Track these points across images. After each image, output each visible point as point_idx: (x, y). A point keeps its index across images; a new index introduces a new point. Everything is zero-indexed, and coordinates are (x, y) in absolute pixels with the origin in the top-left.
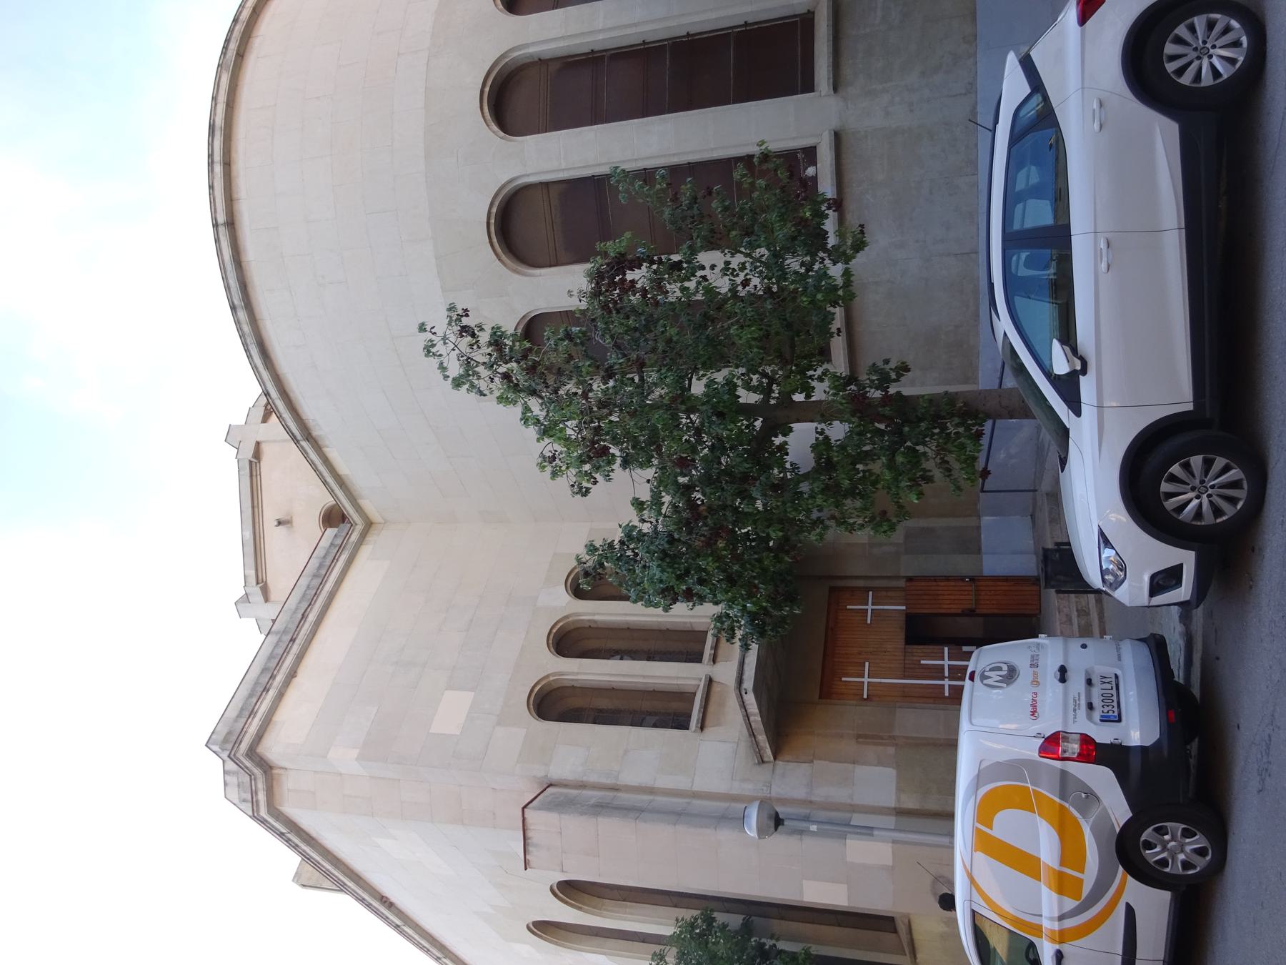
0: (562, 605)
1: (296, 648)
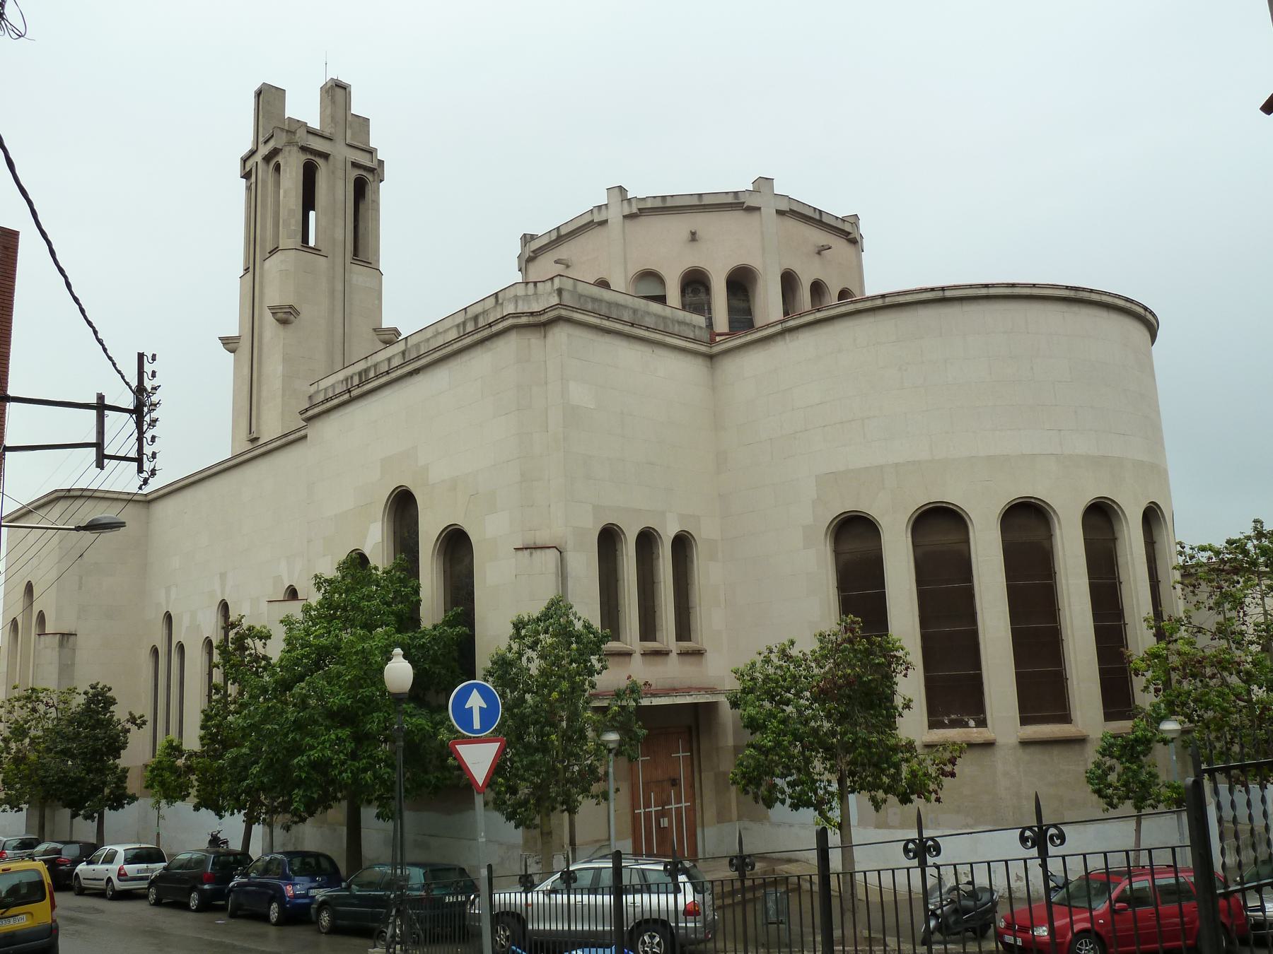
0: (668, 532)
1: (627, 329)
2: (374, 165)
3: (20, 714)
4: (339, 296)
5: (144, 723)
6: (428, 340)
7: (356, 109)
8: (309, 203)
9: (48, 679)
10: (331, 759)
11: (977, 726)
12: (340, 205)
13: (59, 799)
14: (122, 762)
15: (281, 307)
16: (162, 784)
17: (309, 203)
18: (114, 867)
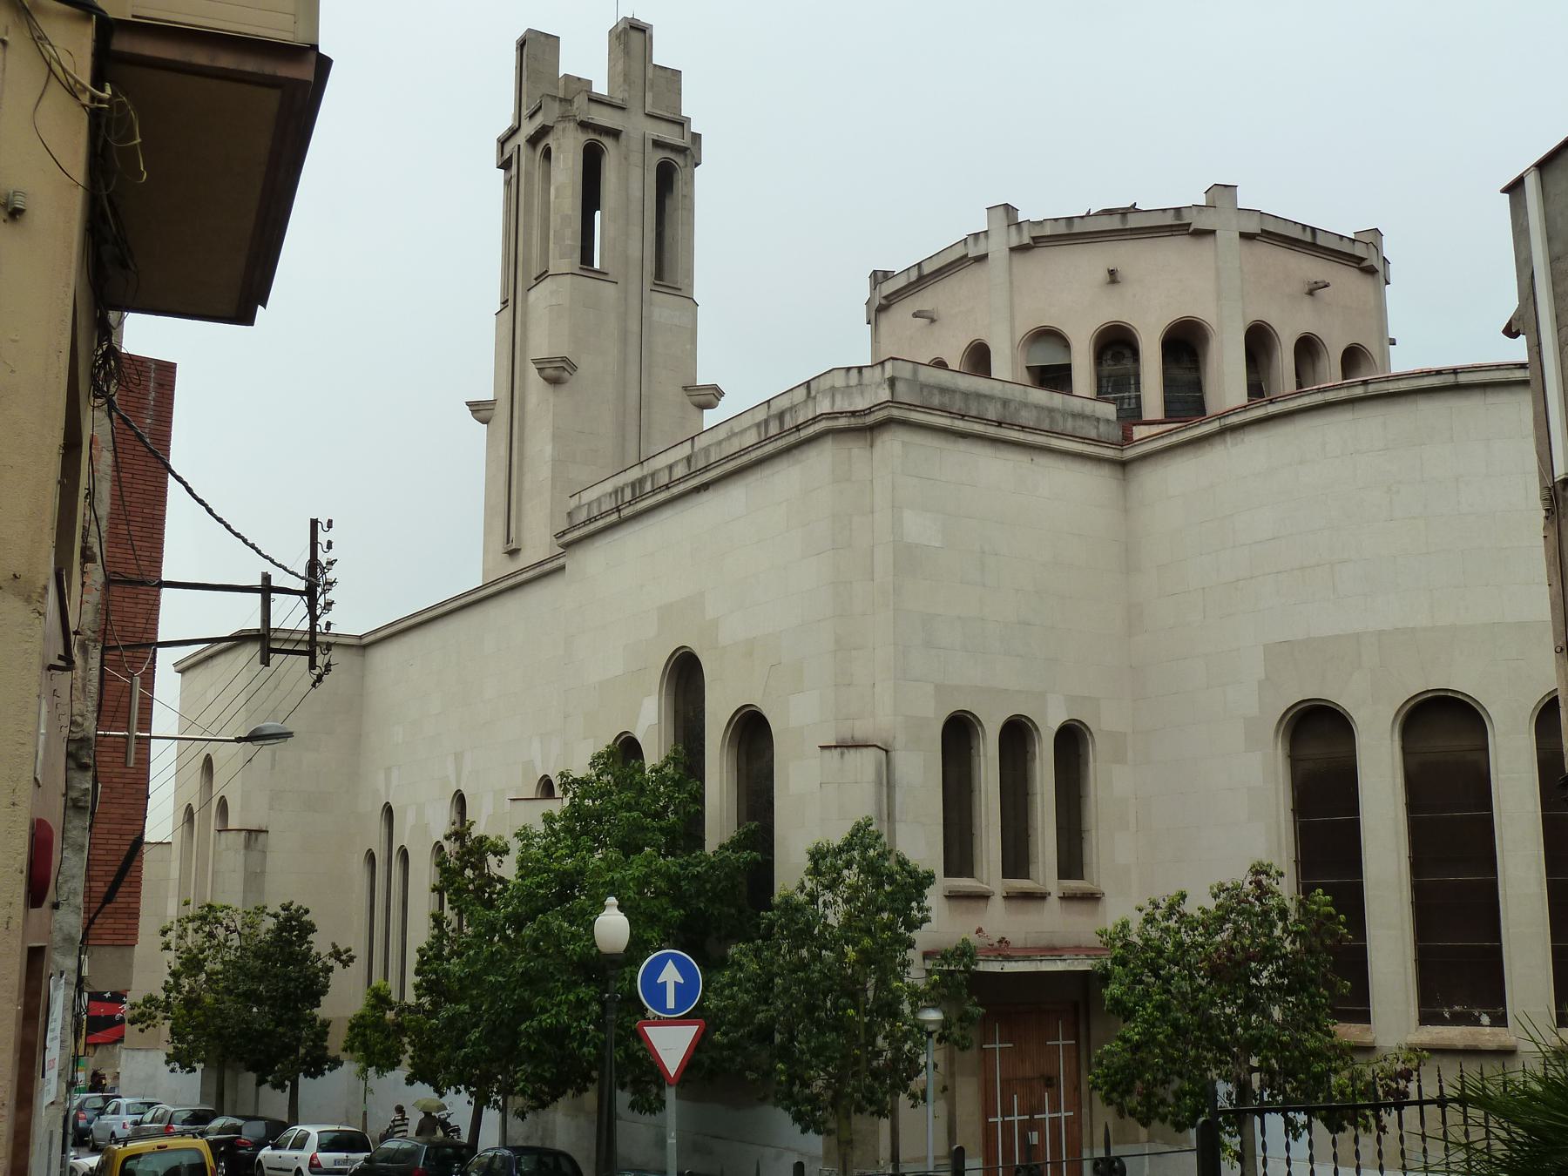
0: (1049, 723)
1: (992, 431)
2: (685, 142)
3: (194, 940)
4: (633, 340)
5: (351, 959)
6: (720, 443)
7: (660, 57)
8: (591, 198)
9: (231, 895)
10: (569, 1027)
11: (1492, 1025)
12: (635, 206)
13: (241, 1059)
14: (321, 1012)
15: (550, 360)
16: (365, 1046)
17: (591, 198)
18: (304, 1155)
